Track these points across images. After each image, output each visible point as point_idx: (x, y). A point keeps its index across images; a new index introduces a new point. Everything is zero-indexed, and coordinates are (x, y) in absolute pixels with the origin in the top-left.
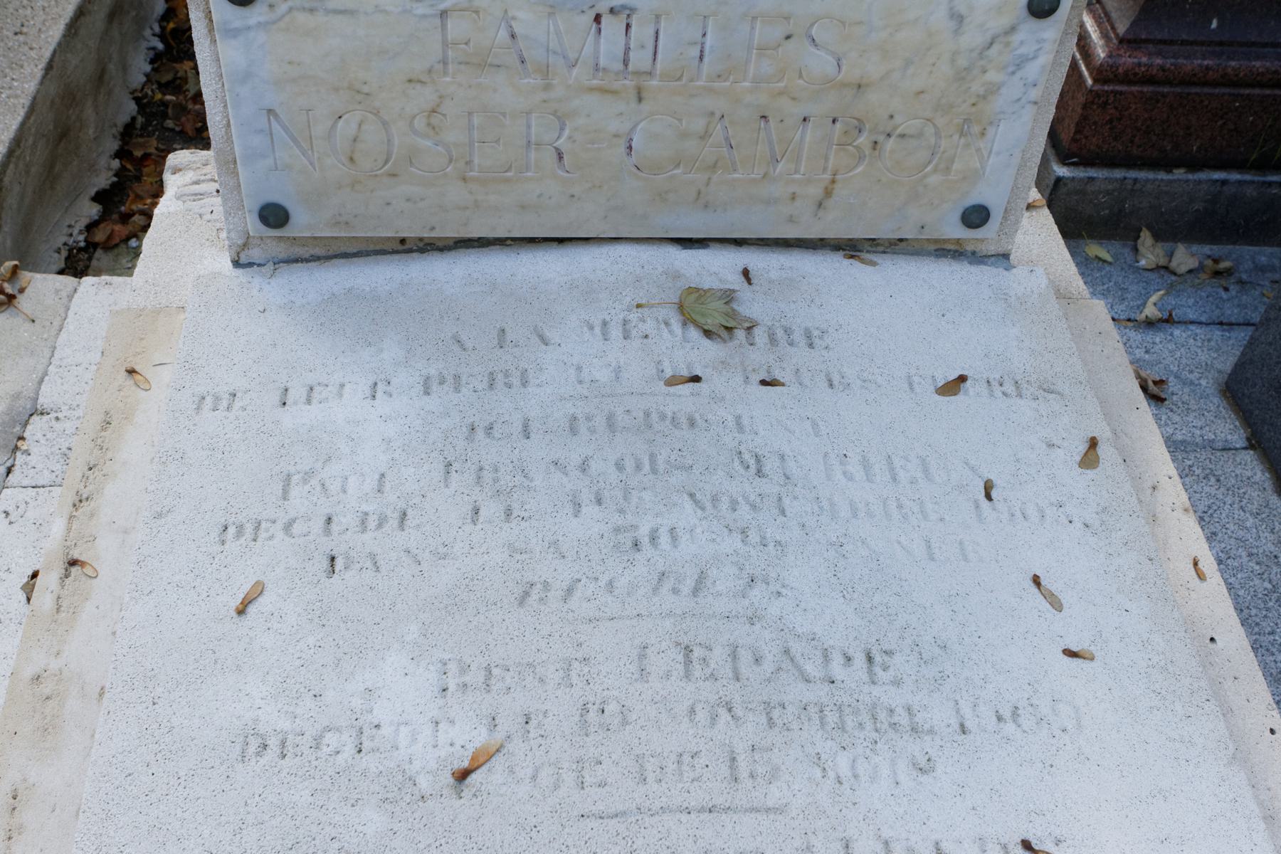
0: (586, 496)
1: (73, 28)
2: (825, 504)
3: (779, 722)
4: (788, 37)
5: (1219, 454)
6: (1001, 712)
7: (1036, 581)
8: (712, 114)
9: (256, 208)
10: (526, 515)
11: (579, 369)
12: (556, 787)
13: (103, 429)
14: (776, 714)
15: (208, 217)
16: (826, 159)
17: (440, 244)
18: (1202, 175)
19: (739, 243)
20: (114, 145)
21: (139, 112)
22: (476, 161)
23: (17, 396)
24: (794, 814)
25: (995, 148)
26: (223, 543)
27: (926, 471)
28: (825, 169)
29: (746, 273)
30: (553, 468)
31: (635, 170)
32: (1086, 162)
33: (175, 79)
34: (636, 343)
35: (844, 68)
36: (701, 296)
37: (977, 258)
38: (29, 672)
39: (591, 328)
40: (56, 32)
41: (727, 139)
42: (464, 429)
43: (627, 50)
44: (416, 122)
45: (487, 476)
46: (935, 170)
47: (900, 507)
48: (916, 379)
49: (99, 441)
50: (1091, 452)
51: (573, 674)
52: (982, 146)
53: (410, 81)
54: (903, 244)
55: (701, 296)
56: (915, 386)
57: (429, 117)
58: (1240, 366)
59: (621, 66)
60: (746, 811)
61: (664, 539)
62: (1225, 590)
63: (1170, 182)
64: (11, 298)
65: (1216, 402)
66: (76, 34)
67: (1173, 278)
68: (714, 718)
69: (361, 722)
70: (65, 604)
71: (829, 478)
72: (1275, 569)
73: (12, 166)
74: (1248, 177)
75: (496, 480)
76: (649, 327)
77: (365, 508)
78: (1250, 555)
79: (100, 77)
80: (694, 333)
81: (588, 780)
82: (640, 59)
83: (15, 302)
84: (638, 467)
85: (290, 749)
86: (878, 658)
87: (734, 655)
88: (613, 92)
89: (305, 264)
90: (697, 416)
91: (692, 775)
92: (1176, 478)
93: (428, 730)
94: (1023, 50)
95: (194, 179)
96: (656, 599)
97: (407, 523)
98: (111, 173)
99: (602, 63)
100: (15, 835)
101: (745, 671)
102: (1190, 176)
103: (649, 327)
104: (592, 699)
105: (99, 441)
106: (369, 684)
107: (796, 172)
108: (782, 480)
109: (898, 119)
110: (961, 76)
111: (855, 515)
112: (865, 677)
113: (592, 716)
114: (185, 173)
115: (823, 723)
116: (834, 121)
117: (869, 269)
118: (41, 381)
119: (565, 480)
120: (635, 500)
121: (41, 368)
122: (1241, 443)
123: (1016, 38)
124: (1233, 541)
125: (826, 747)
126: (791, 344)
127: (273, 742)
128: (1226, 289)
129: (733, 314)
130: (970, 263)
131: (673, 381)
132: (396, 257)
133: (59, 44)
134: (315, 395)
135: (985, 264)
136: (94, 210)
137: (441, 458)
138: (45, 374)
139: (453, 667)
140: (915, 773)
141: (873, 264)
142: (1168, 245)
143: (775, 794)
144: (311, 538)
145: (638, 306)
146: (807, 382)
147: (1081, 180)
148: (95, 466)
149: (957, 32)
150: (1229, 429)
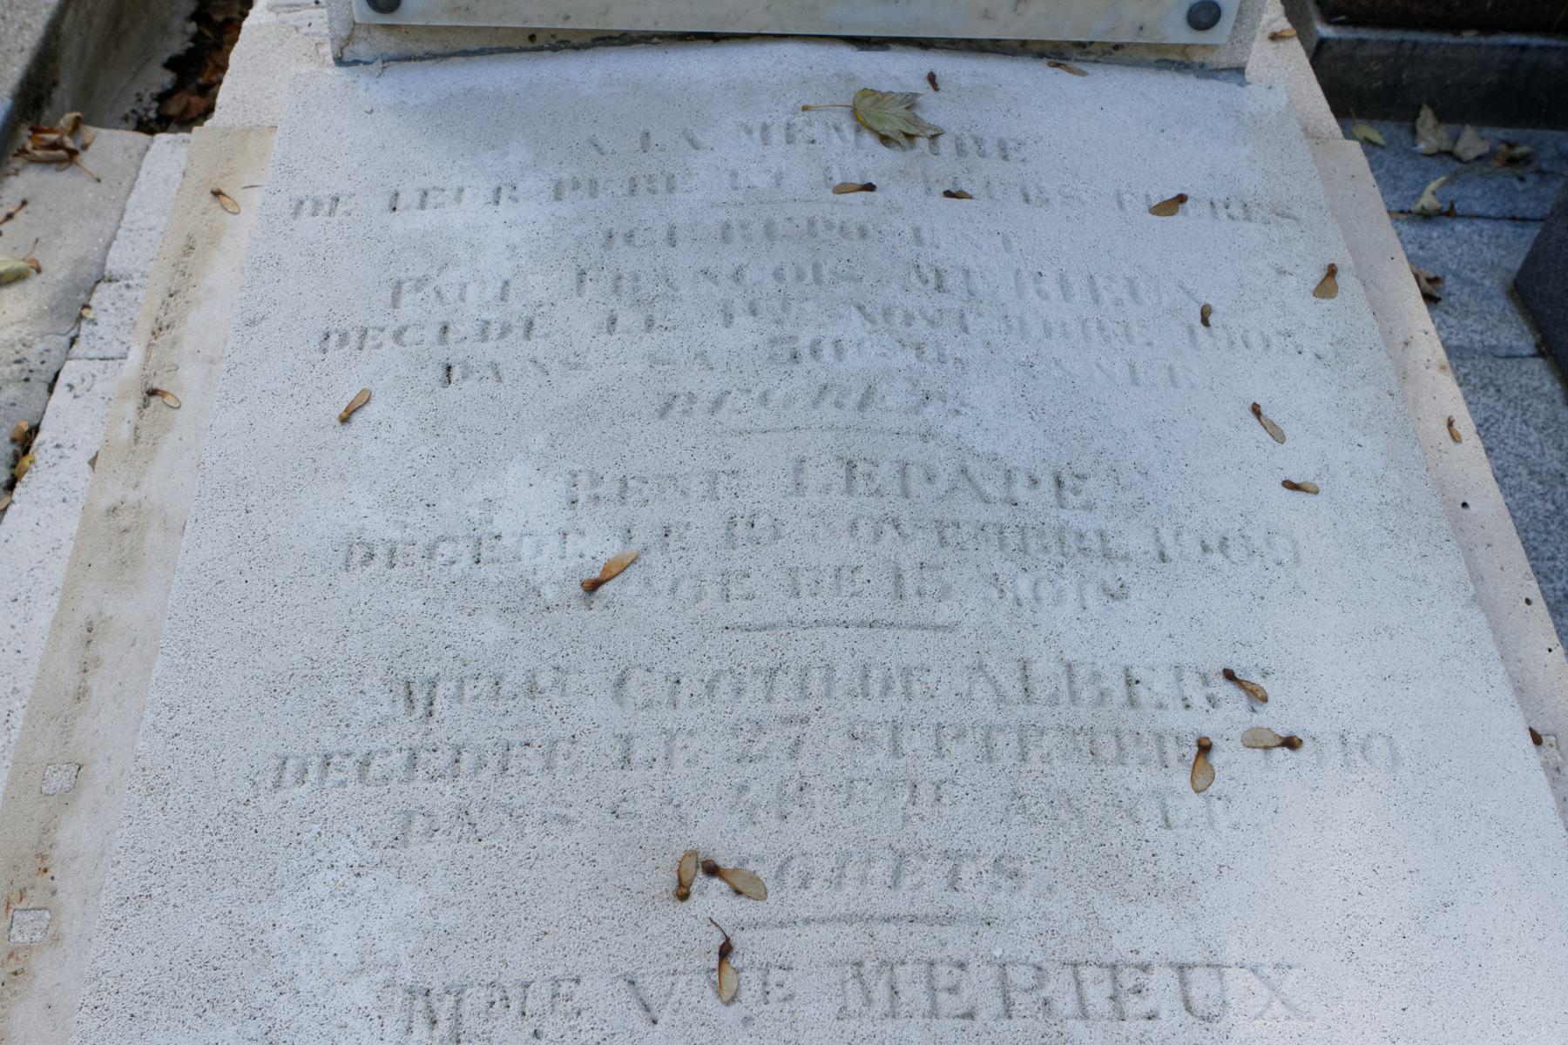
0: (739, 306)
2: (1015, 323)
3: (953, 541)
5: (1501, 362)
7: (1256, 410)
10: (669, 324)
11: (734, 174)
12: (698, 600)
13: (186, 254)
14: (949, 533)
15: (306, 30)
17: (576, 41)
18: (1497, 39)
19: (925, 44)
23: (80, 262)
26: (325, 351)
27: (1134, 293)
29: (932, 78)
32: (1355, 21)
37: (1206, 71)
38: (104, 502)
39: (749, 132)
45: (626, 285)
47: (1101, 329)
48: (1127, 197)
51: (720, 487)
54: (1119, 53)
56: (1126, 204)
58: (1531, 259)
60: (912, 627)
61: (827, 351)
62: (1483, 454)
63: (1457, 47)
64: (73, 153)
65: (1501, 303)
67: (1458, 165)
68: (879, 534)
69: (479, 532)
71: (1020, 296)
72: (1560, 489)
73: (71, 12)
74: (1553, 42)
75: (636, 290)
76: (817, 131)
77: (485, 316)
78: (1531, 473)
80: (869, 140)
81: (734, 591)
83: (78, 158)
84: (800, 277)
86: (1069, 482)
87: (904, 472)
89: (418, 63)
91: (851, 590)
92: (1433, 333)
93: (554, 542)
96: (814, 412)
97: (535, 332)
98: (186, 38)
100: (91, 669)
101: (914, 487)
102: (1482, 40)
103: (817, 131)
104: (740, 512)
108: (965, 296)
111: (1048, 334)
112: (1053, 500)
113: (741, 529)
115: (1002, 545)
117: (1077, 79)
118: (109, 246)
119: (715, 288)
120: (794, 311)
121: (108, 232)
122: (1530, 350)
124: (1511, 458)
125: (1005, 568)
126: (983, 156)
127: (381, 551)
128: (1522, 179)
129: (916, 121)
131: (843, 189)
132: (525, 55)
134: (430, 200)
135: (1216, 78)
136: (167, 79)
138: (114, 237)
139: (583, 478)
140: (1105, 599)
141: (1083, 74)
142: (1454, 128)
143: (945, 613)
144: (425, 346)
145: (805, 109)
147: (1350, 42)
150: (1515, 335)
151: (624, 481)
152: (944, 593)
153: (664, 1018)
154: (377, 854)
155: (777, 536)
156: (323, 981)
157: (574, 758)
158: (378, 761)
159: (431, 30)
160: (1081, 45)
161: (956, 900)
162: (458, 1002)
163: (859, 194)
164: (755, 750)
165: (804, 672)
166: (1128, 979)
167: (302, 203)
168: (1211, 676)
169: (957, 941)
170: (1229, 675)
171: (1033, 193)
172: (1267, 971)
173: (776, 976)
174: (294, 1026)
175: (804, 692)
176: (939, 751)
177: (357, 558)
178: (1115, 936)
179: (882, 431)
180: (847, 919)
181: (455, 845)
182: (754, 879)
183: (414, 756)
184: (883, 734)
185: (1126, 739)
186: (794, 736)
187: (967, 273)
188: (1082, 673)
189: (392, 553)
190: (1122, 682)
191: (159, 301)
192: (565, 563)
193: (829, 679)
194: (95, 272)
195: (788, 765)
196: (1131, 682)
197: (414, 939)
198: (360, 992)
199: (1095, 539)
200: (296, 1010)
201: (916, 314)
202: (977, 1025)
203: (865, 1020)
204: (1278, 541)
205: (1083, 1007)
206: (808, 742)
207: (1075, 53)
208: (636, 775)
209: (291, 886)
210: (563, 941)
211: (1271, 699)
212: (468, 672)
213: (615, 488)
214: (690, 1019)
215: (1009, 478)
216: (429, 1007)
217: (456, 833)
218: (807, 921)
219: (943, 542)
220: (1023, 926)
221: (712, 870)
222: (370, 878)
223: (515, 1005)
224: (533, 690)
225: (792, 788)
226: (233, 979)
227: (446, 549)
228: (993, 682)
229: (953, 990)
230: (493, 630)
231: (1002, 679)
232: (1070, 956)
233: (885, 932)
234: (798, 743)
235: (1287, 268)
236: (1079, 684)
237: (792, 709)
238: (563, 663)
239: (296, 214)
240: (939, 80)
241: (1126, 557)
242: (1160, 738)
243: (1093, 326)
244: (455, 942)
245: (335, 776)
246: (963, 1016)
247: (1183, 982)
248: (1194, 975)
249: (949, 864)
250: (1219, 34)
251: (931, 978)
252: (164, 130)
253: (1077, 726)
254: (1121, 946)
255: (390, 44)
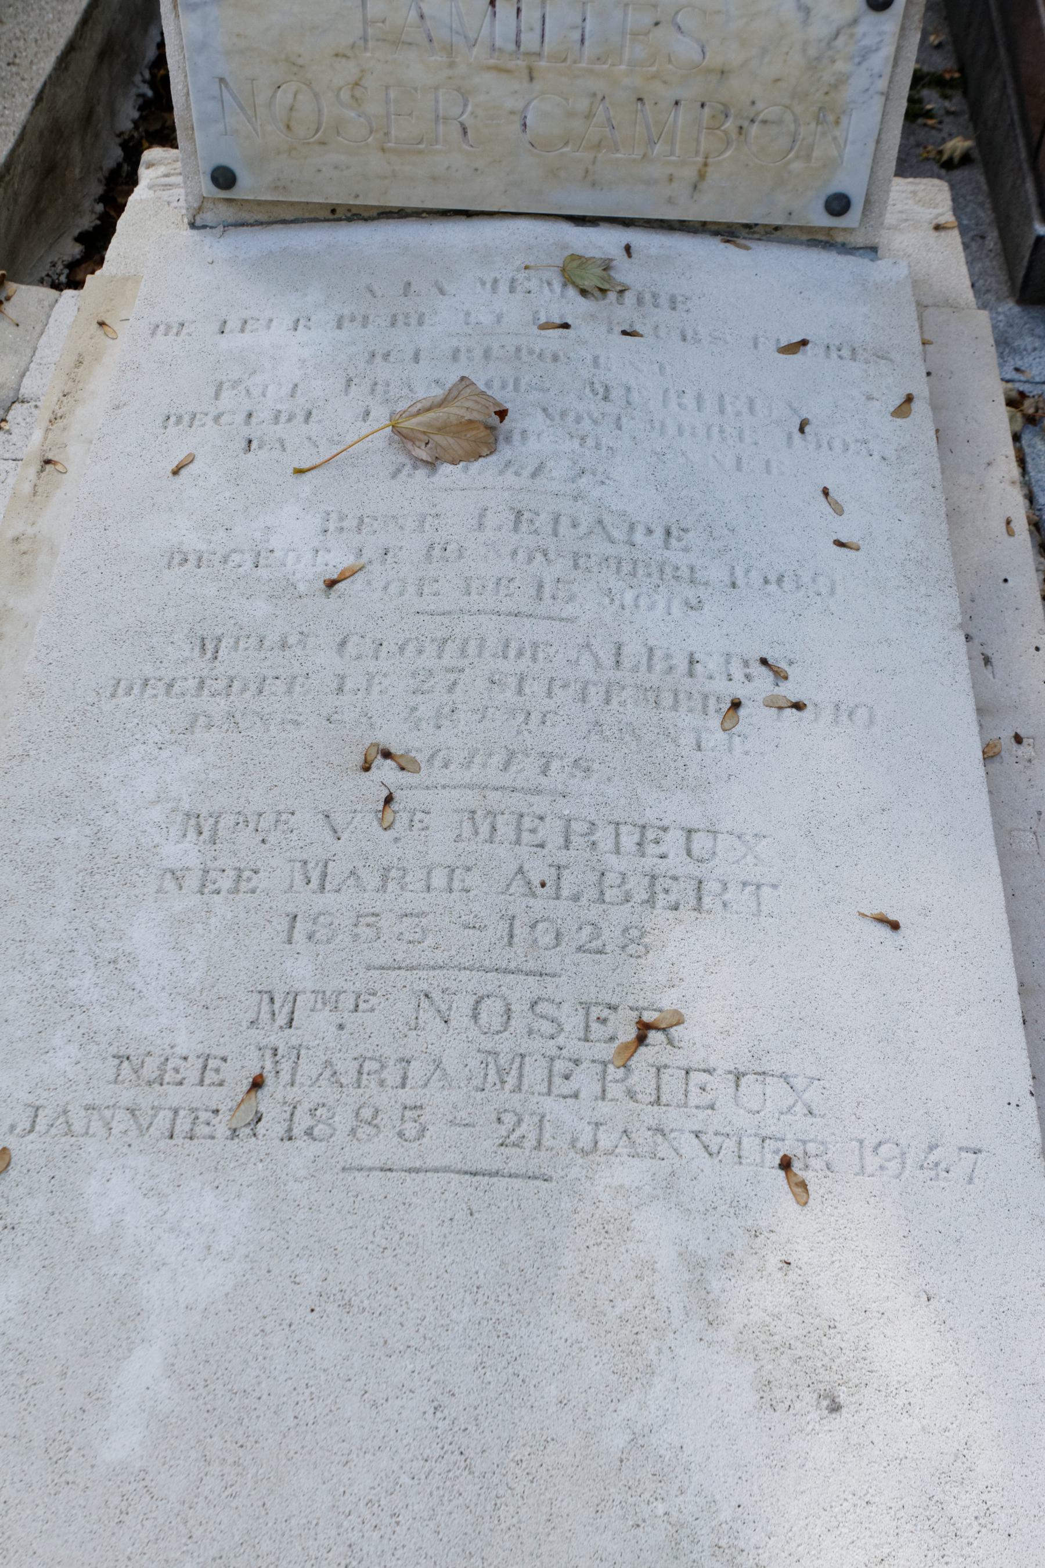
1: (64, 61)
2: (657, 425)
4: (657, 24)
6: (769, 577)
7: (826, 492)
8: (595, 95)
9: (209, 171)
11: (468, 314)
12: (401, 594)
13: (77, 367)
14: (581, 561)
15: (175, 204)
16: (698, 141)
17: (366, 215)
19: (627, 223)
20: (98, 189)
21: (125, 159)
22: (393, 133)
24: (581, 624)
25: (850, 137)
26: (166, 428)
27: (752, 410)
28: (697, 153)
29: (628, 249)
30: (433, 385)
31: (530, 146)
33: (163, 128)
34: (519, 296)
35: (708, 54)
36: (582, 263)
37: (846, 249)
39: (483, 284)
40: (47, 65)
41: (609, 120)
42: (366, 354)
43: (518, 33)
44: (342, 93)
45: (379, 389)
46: (797, 157)
47: (721, 432)
48: (762, 340)
49: (73, 375)
50: (906, 406)
52: (838, 134)
53: (337, 55)
54: (779, 233)
55: (582, 263)
56: (760, 345)
57: (352, 89)
59: (513, 47)
60: (544, 618)
66: (66, 68)
68: (531, 559)
69: (259, 548)
70: (40, 490)
71: (665, 406)
77: (279, 407)
79: (88, 118)
80: (572, 292)
81: (426, 590)
82: (530, 41)
85: (204, 563)
86: (675, 532)
87: (556, 521)
88: (508, 71)
89: (249, 228)
90: (561, 354)
91: (506, 592)
93: (309, 555)
94: (865, 42)
95: (165, 172)
97: (312, 419)
98: (94, 216)
99: (498, 43)
105: (73, 375)
106: (269, 524)
107: (672, 153)
109: (760, 105)
110: (813, 65)
112: (661, 544)
113: (437, 552)
114: (156, 166)
115: (618, 571)
116: (703, 105)
117: (743, 252)
118: (23, 375)
121: (23, 364)
123: (860, 29)
129: (609, 279)
130: (839, 253)
131: (545, 327)
132: (327, 224)
133: (50, 77)
134: (248, 327)
137: (345, 374)
138: (27, 369)
139: (334, 516)
140: (685, 608)
141: (747, 248)
143: (569, 610)
144: (234, 426)
145: (526, 268)
146: (662, 335)
148: (68, 393)
149: (805, 22)
151: (361, 520)
152: (571, 598)
153: (344, 837)
154: (173, 737)
155: (461, 556)
156: (134, 806)
157: (306, 687)
158: (179, 683)
159: (259, 203)
160: (748, 226)
161: (544, 781)
162: (217, 822)
163: (556, 330)
164: (425, 687)
165: (466, 642)
166: (650, 835)
167: (158, 326)
168: (751, 662)
169: (540, 804)
170: (764, 662)
171: (689, 334)
172: (748, 838)
173: (419, 816)
174: (114, 830)
175: (463, 652)
176: (549, 694)
177: (176, 561)
178: (648, 809)
179: (546, 492)
180: (470, 787)
181: (223, 734)
182: (414, 761)
183: (202, 682)
184: (513, 682)
185: (681, 696)
186: (452, 679)
187: (628, 389)
188: (658, 654)
189: (200, 559)
190: (686, 661)
191: (55, 399)
192: (315, 569)
193: (481, 647)
194: (11, 395)
195: (446, 696)
196: (692, 661)
197: (192, 786)
198: (156, 814)
199: (686, 570)
200: (115, 821)
201: (585, 415)
202: (545, 851)
203: (472, 842)
204: (821, 580)
205: (617, 844)
206: (461, 683)
207: (744, 232)
208: (346, 699)
209: (117, 753)
210: (287, 791)
211: (790, 678)
212: (243, 633)
213: (355, 523)
214: (361, 837)
215: (632, 527)
216: (198, 824)
217: (225, 727)
218: (444, 787)
219: (576, 566)
220: (586, 799)
221: (387, 755)
222: (168, 751)
223: (252, 825)
224: (284, 646)
225: (446, 710)
226: (77, 802)
227: (236, 558)
228: (596, 656)
229: (533, 831)
230: (261, 608)
231: (601, 654)
232: (616, 818)
233: (493, 796)
234: (455, 683)
235: (875, 395)
236: (656, 659)
237: (454, 663)
238: (306, 630)
239: (153, 334)
240: (632, 250)
241: (706, 584)
242: (706, 697)
243: (715, 430)
244: (218, 789)
245: (150, 691)
246: (537, 846)
247: (689, 839)
248: (695, 836)
249: (544, 760)
250: (852, 219)
251: (519, 824)
252: (70, 288)
253: (648, 686)
254: (650, 816)
255: (228, 213)
